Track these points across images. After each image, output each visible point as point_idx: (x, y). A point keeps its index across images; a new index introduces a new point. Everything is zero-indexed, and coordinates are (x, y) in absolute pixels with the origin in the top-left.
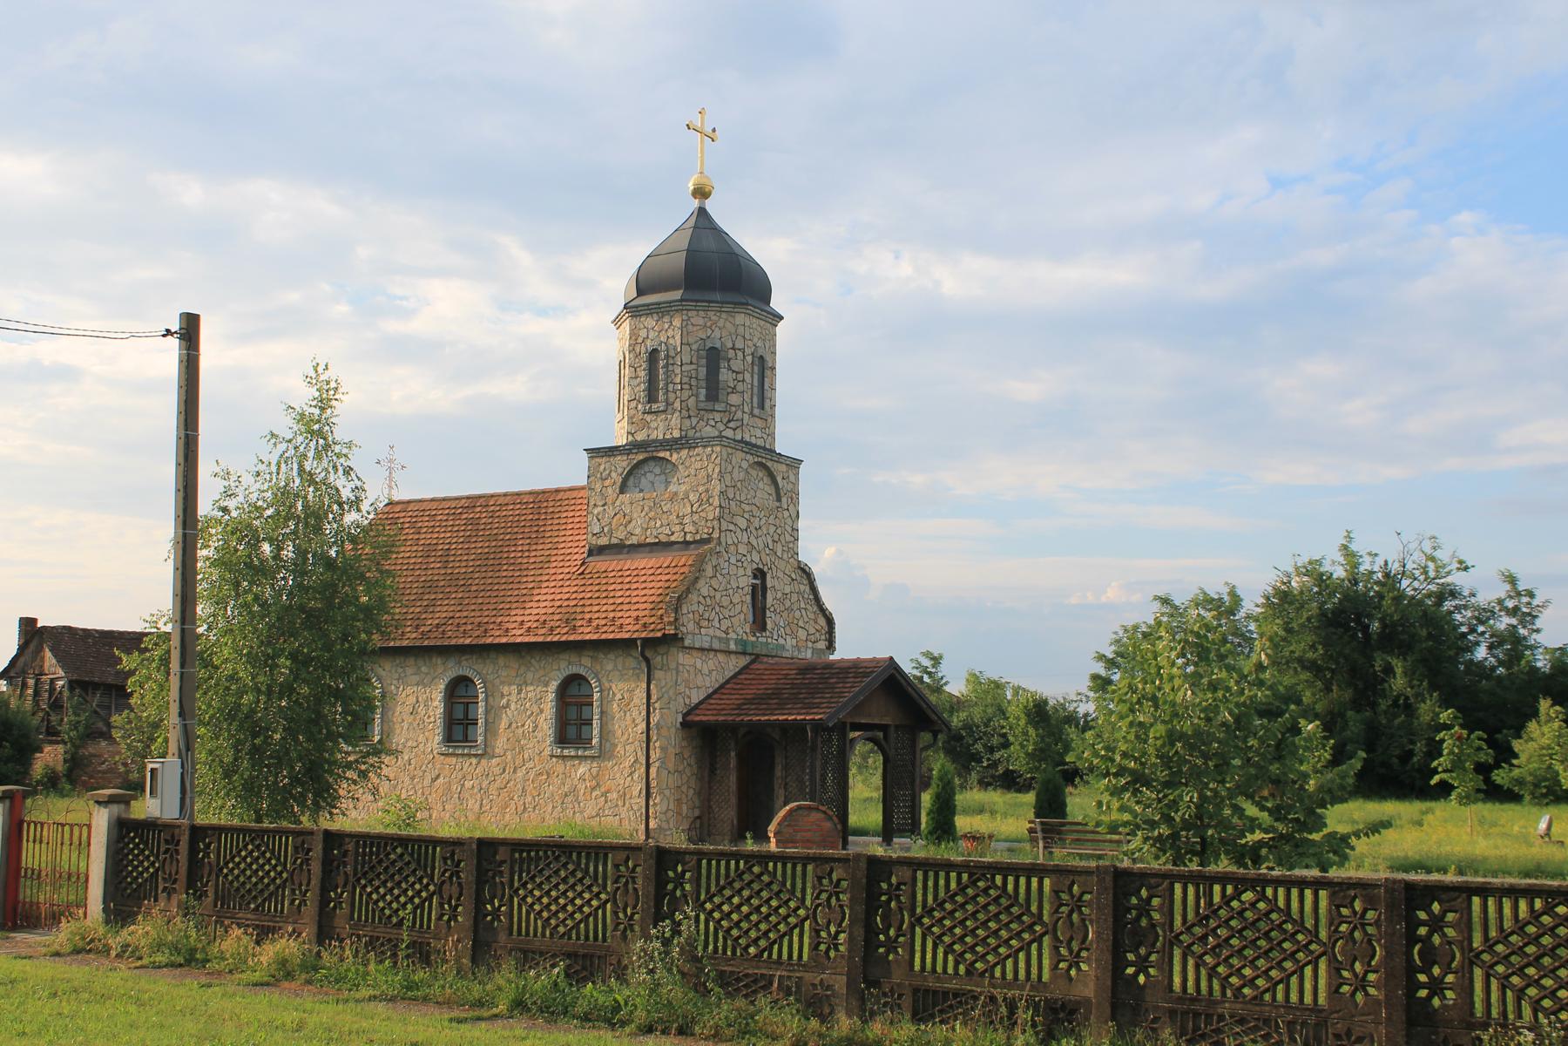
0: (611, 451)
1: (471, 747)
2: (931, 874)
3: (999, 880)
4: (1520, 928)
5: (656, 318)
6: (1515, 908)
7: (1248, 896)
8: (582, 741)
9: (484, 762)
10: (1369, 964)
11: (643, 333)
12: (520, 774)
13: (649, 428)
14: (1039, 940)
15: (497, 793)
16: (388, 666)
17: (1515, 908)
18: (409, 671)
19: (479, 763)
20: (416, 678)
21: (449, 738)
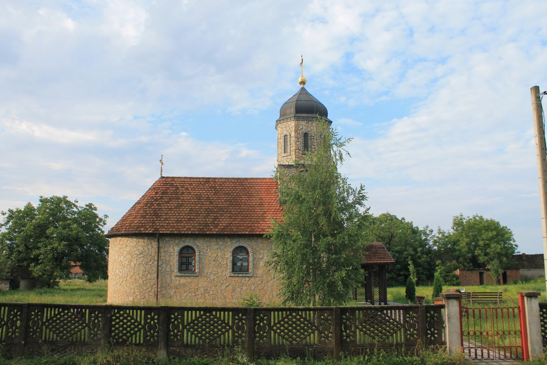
0: (289, 166)
1: (246, 273)
2: (49, 309)
3: (128, 311)
4: (283, 319)
5: (306, 122)
6: (282, 314)
7: (122, 312)
8: (187, 269)
9: (252, 279)
10: (155, 330)
11: (301, 127)
12: (269, 284)
13: (304, 160)
14: (228, 331)
15: (259, 291)
16: (201, 241)
17: (282, 314)
18: (212, 244)
19: (250, 280)
20: (216, 247)
21: (180, 270)
